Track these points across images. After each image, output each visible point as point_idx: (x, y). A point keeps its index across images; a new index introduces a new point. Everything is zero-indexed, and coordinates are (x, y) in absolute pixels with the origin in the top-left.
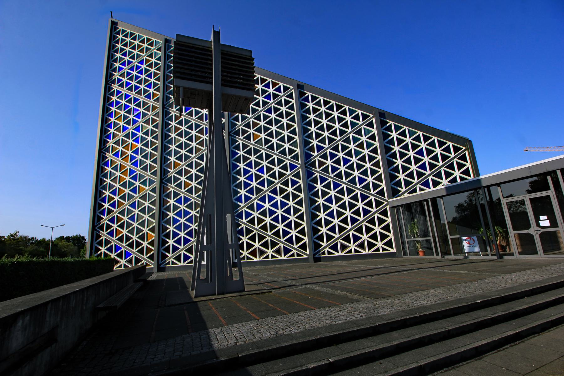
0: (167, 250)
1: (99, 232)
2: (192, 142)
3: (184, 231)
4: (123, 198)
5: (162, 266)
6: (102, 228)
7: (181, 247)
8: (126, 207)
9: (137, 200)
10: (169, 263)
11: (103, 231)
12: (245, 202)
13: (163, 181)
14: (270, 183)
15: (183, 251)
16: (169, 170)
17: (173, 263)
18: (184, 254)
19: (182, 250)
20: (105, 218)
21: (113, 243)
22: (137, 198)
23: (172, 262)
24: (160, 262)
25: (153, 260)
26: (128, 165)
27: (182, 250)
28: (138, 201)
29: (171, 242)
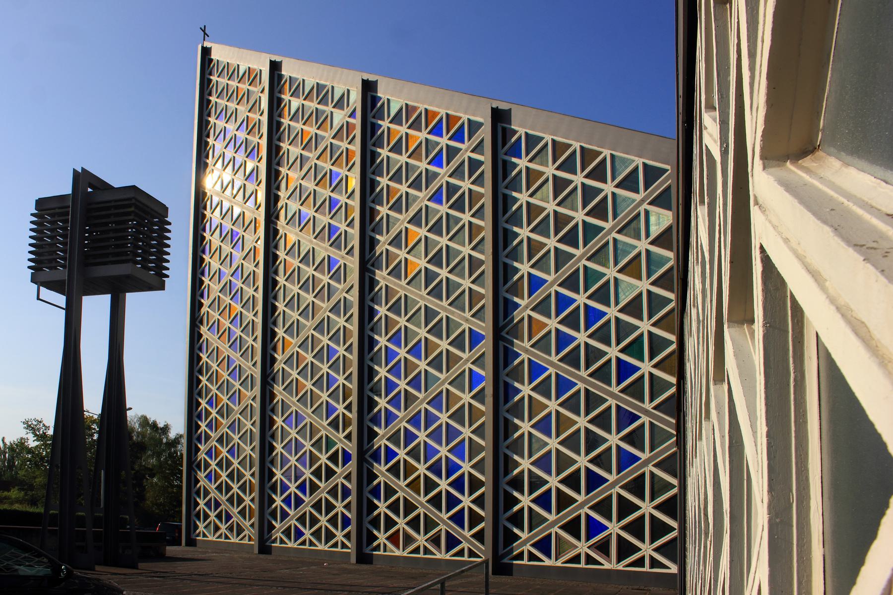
0: (517, 520)
1: (372, 466)
2: (605, 182)
3: (618, 432)
4: (436, 363)
5: (506, 560)
6: (376, 456)
7: (581, 498)
8: (581, 265)
9: (552, 290)
10: (520, 556)
11: (380, 463)
12: (619, 472)
13: (503, 334)
14: (626, 460)
15: (617, 489)
16: (516, 299)
17: (532, 557)
18: (620, 496)
19: (646, 462)
20: (522, 303)
21: (551, 370)
22: (609, 232)
23: (530, 553)
24: (501, 552)
25: (482, 543)
26: (421, 297)
27: (646, 462)
28: (470, 370)
29: (525, 501)
